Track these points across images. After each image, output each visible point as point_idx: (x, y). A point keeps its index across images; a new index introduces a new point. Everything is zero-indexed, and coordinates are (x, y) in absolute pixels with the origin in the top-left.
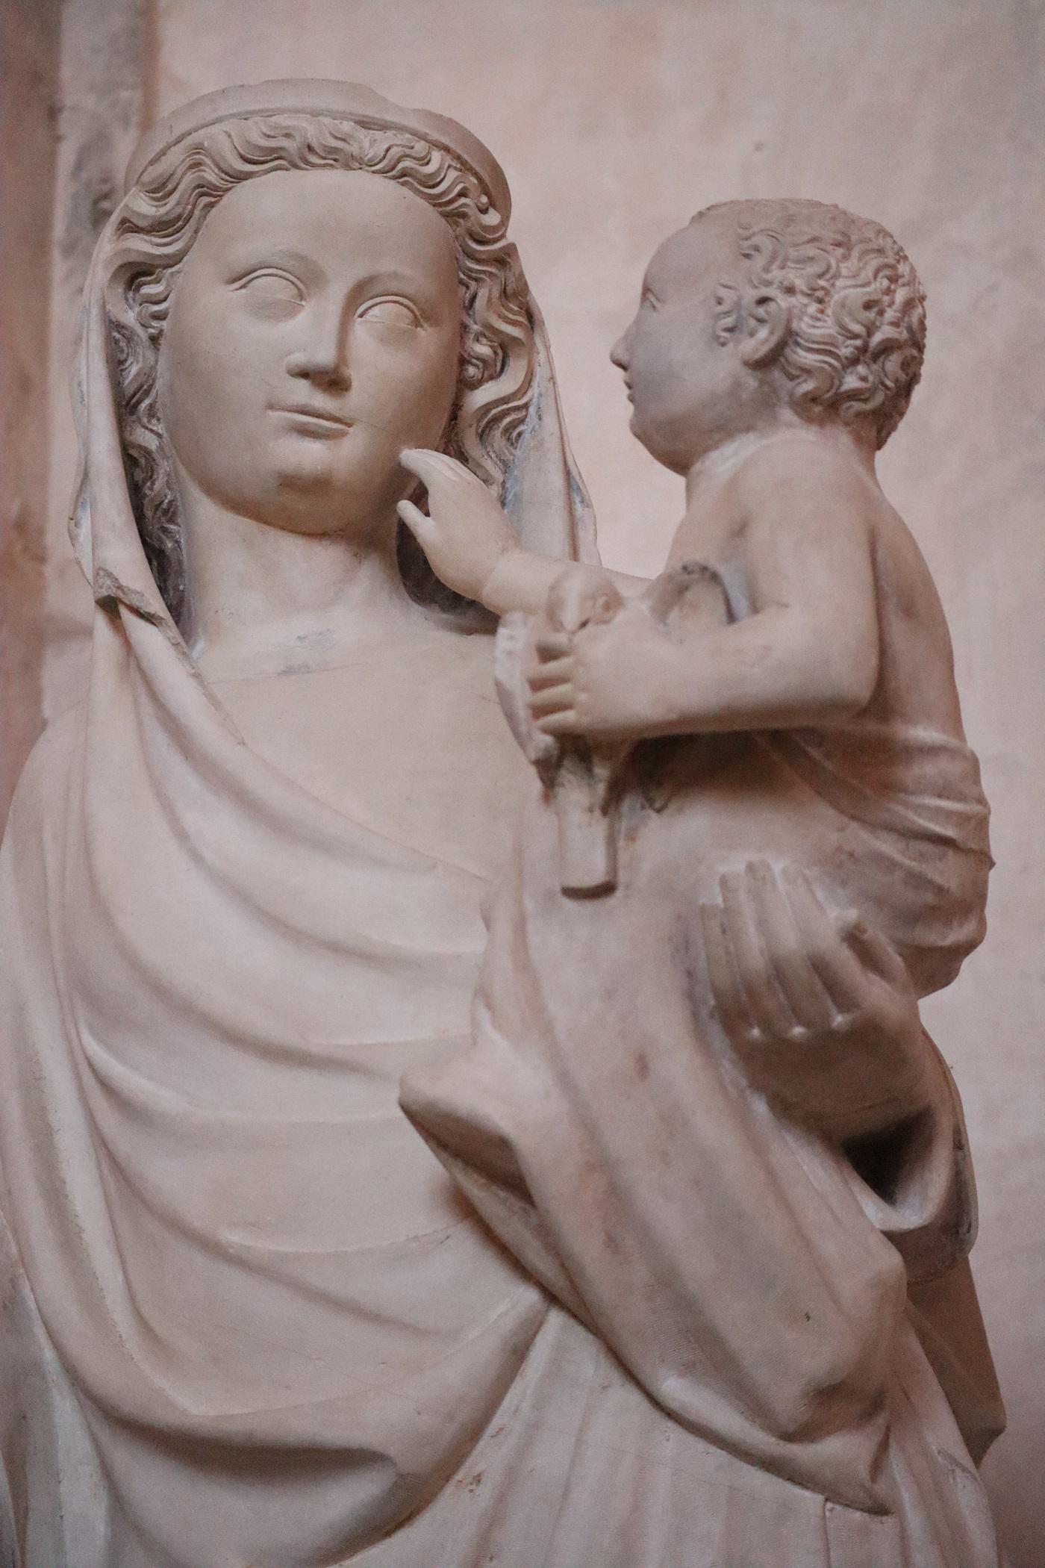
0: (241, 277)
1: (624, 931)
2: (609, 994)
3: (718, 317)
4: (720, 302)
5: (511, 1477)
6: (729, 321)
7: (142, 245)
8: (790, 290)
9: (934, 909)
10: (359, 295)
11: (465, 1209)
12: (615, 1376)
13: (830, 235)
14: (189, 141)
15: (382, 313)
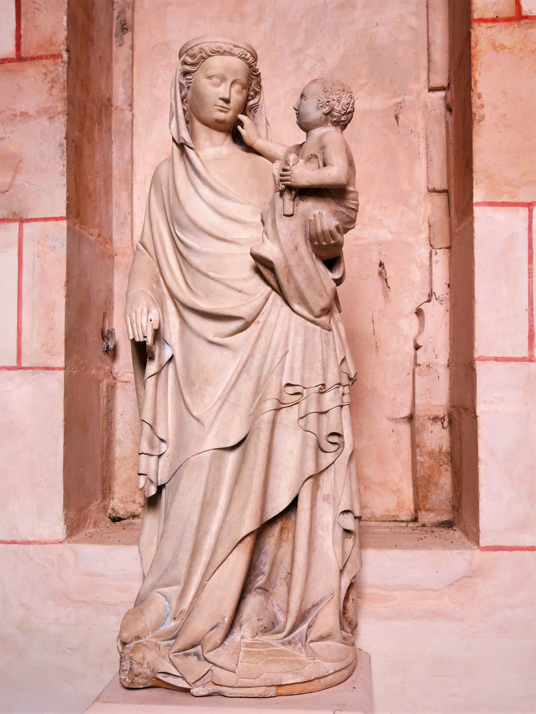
0: (210, 77)
1: (294, 224)
2: (291, 235)
3: (318, 104)
4: (319, 101)
5: (265, 322)
6: (321, 105)
7: (188, 68)
8: (333, 100)
9: (350, 222)
10: (233, 83)
11: (257, 271)
12: (284, 304)
13: (341, 89)
14: (199, 46)
15: (237, 87)
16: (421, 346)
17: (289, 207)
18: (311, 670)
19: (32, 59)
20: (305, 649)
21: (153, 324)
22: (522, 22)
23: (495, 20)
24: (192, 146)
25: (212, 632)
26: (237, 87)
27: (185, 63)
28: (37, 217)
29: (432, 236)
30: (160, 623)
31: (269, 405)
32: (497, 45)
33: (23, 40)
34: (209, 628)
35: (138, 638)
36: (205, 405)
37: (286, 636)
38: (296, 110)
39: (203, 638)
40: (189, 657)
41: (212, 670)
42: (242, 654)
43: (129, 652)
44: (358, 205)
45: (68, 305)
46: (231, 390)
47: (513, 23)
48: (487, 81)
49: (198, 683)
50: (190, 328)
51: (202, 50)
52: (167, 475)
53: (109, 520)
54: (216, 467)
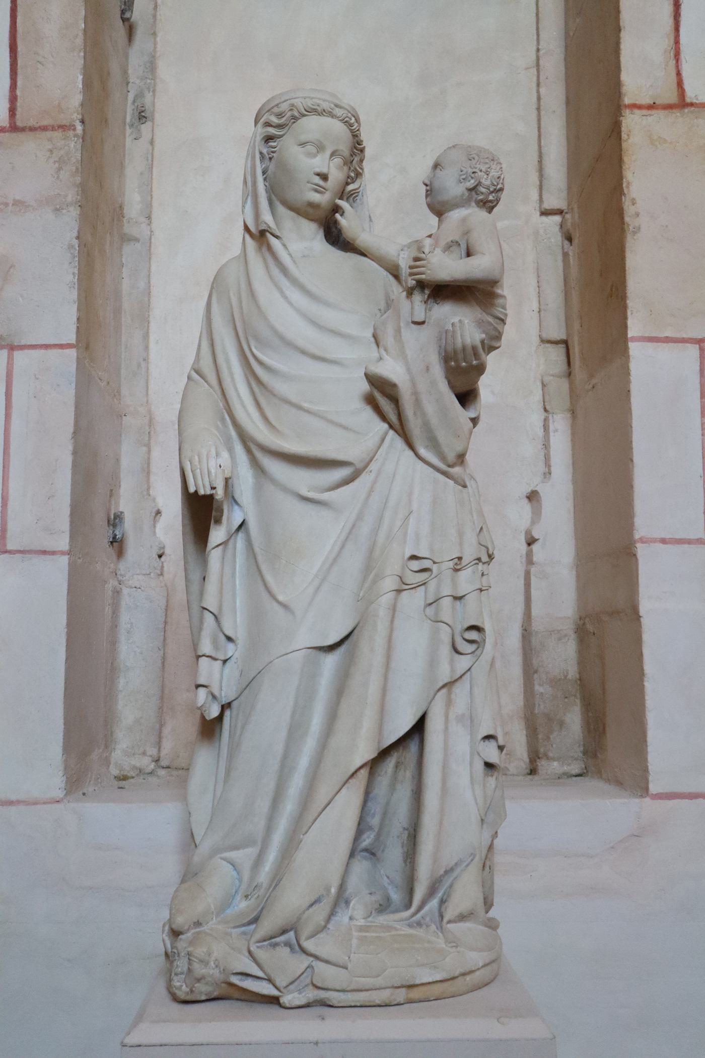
0: (302, 144)
1: (426, 335)
7: (272, 131)
8: (481, 171)
10: (333, 154)
11: (370, 400)
13: (491, 157)
14: (288, 102)
16: (537, 540)
18: (452, 963)
19: (32, 129)
20: (442, 932)
21: (224, 471)
22: (686, 110)
23: (651, 107)
24: (278, 234)
25: (311, 910)
26: (338, 161)
27: (268, 124)
28: (34, 343)
29: (547, 398)
30: (226, 903)
31: (389, 584)
32: (655, 138)
34: (307, 904)
35: (198, 924)
36: (295, 584)
38: (426, 185)
39: (299, 919)
40: (277, 948)
41: (313, 967)
42: (355, 942)
43: (185, 946)
44: (506, 315)
45: (75, 465)
46: (332, 565)
47: (674, 111)
48: (647, 183)
49: (291, 987)
50: (273, 481)
52: (235, 689)
54: (310, 676)
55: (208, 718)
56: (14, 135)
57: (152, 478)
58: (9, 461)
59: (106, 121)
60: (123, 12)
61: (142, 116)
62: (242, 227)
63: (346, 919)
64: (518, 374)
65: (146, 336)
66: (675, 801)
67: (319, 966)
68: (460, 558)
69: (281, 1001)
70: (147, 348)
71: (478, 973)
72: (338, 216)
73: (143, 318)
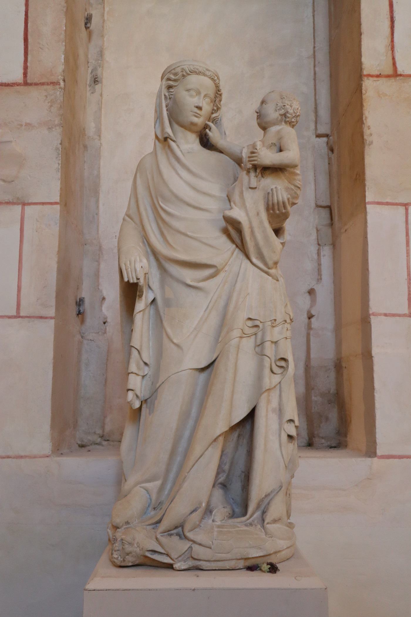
0: (188, 90)
7: (171, 83)
10: (205, 96)
11: (225, 231)
17: (254, 182)
19: (36, 84)
22: (398, 78)
23: (378, 76)
24: (174, 139)
26: (208, 100)
27: (169, 79)
31: (236, 333)
33: (29, 70)
34: (190, 512)
35: (127, 523)
37: (248, 520)
38: (257, 113)
40: (172, 537)
49: (180, 558)
50: (172, 276)
51: (183, 70)
53: (77, 446)
55: (133, 408)
56: (26, 87)
57: (101, 280)
58: (22, 267)
59: (77, 82)
60: (86, 24)
61: (96, 81)
62: (154, 137)
63: (210, 521)
64: (304, 224)
65: (97, 201)
66: (391, 460)
67: (196, 547)
68: (275, 320)
69: (174, 566)
70: (98, 207)
71: (283, 552)
72: (207, 130)
73: (96, 191)
